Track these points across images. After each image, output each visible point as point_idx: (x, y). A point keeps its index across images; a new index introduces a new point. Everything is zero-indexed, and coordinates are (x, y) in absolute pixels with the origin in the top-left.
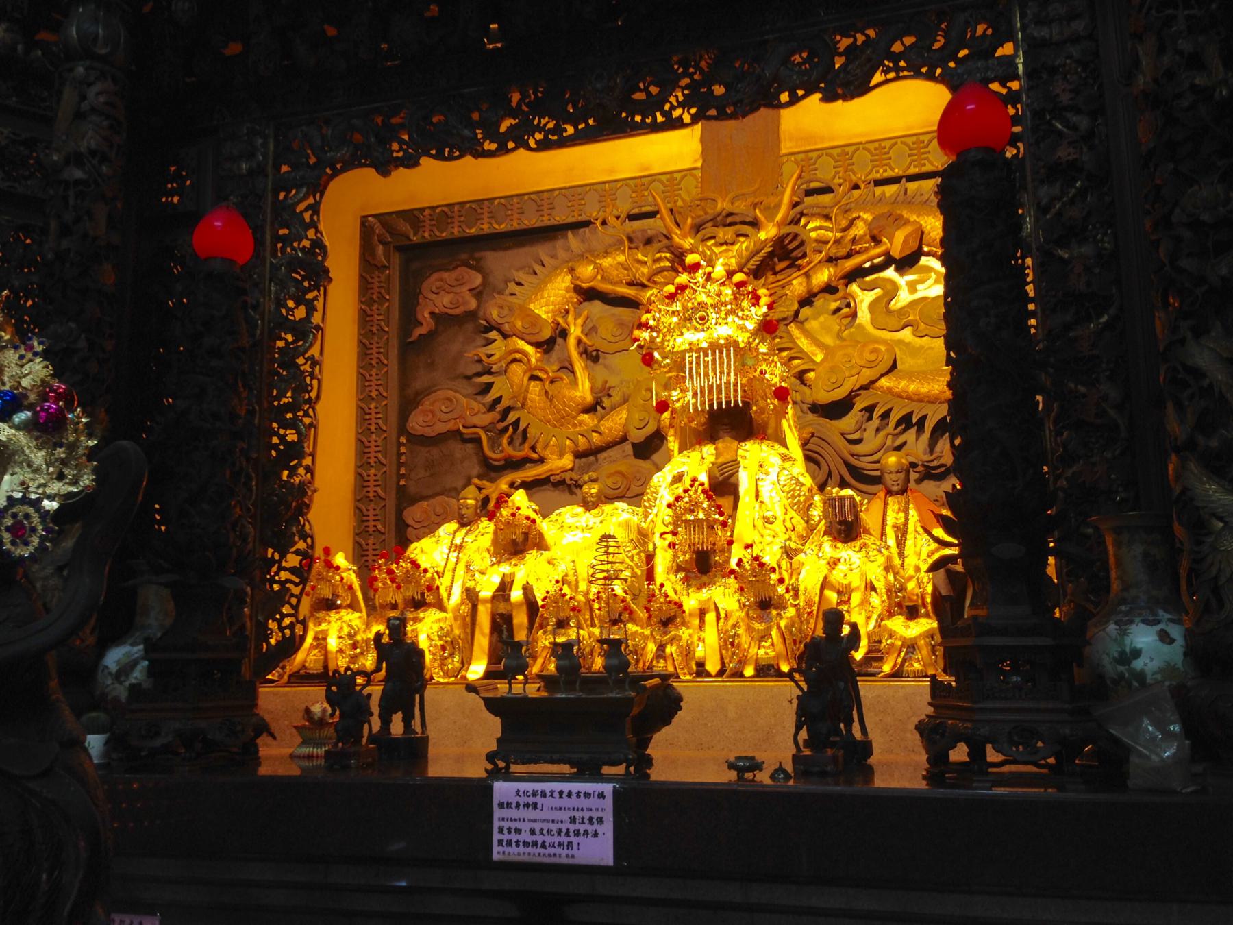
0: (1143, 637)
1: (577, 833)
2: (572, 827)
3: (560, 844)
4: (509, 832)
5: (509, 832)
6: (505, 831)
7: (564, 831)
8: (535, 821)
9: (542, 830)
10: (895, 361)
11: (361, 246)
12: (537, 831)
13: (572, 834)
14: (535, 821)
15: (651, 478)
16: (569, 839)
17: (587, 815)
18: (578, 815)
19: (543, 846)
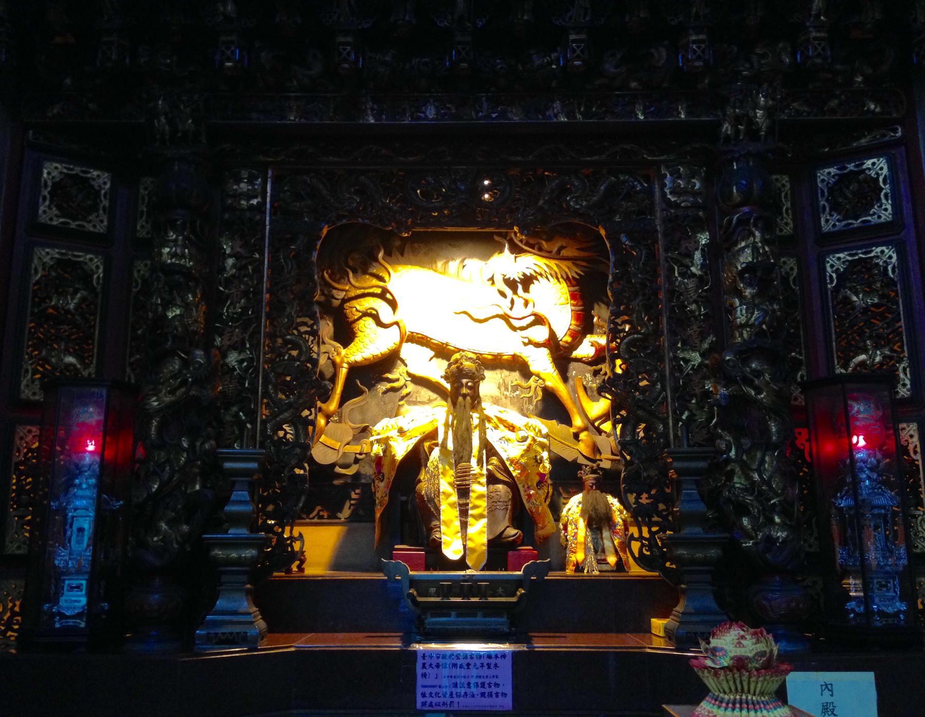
0: (185, 527)
1: (458, 695)
2: (454, 690)
3: (444, 704)
4: (490, 687)
5: (490, 687)
6: (486, 686)
7: (449, 693)
8: (426, 686)
9: (431, 693)
10: (498, 316)
11: (878, 700)
12: (427, 695)
13: (454, 695)
14: (426, 686)
15: (334, 326)
16: (452, 700)
17: (487, 681)
18: (487, 681)
19: (431, 705)
